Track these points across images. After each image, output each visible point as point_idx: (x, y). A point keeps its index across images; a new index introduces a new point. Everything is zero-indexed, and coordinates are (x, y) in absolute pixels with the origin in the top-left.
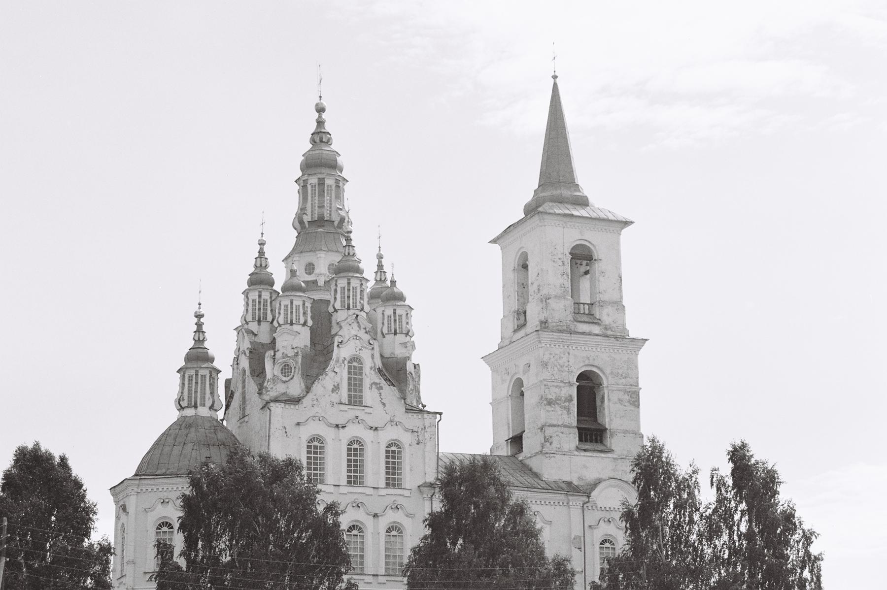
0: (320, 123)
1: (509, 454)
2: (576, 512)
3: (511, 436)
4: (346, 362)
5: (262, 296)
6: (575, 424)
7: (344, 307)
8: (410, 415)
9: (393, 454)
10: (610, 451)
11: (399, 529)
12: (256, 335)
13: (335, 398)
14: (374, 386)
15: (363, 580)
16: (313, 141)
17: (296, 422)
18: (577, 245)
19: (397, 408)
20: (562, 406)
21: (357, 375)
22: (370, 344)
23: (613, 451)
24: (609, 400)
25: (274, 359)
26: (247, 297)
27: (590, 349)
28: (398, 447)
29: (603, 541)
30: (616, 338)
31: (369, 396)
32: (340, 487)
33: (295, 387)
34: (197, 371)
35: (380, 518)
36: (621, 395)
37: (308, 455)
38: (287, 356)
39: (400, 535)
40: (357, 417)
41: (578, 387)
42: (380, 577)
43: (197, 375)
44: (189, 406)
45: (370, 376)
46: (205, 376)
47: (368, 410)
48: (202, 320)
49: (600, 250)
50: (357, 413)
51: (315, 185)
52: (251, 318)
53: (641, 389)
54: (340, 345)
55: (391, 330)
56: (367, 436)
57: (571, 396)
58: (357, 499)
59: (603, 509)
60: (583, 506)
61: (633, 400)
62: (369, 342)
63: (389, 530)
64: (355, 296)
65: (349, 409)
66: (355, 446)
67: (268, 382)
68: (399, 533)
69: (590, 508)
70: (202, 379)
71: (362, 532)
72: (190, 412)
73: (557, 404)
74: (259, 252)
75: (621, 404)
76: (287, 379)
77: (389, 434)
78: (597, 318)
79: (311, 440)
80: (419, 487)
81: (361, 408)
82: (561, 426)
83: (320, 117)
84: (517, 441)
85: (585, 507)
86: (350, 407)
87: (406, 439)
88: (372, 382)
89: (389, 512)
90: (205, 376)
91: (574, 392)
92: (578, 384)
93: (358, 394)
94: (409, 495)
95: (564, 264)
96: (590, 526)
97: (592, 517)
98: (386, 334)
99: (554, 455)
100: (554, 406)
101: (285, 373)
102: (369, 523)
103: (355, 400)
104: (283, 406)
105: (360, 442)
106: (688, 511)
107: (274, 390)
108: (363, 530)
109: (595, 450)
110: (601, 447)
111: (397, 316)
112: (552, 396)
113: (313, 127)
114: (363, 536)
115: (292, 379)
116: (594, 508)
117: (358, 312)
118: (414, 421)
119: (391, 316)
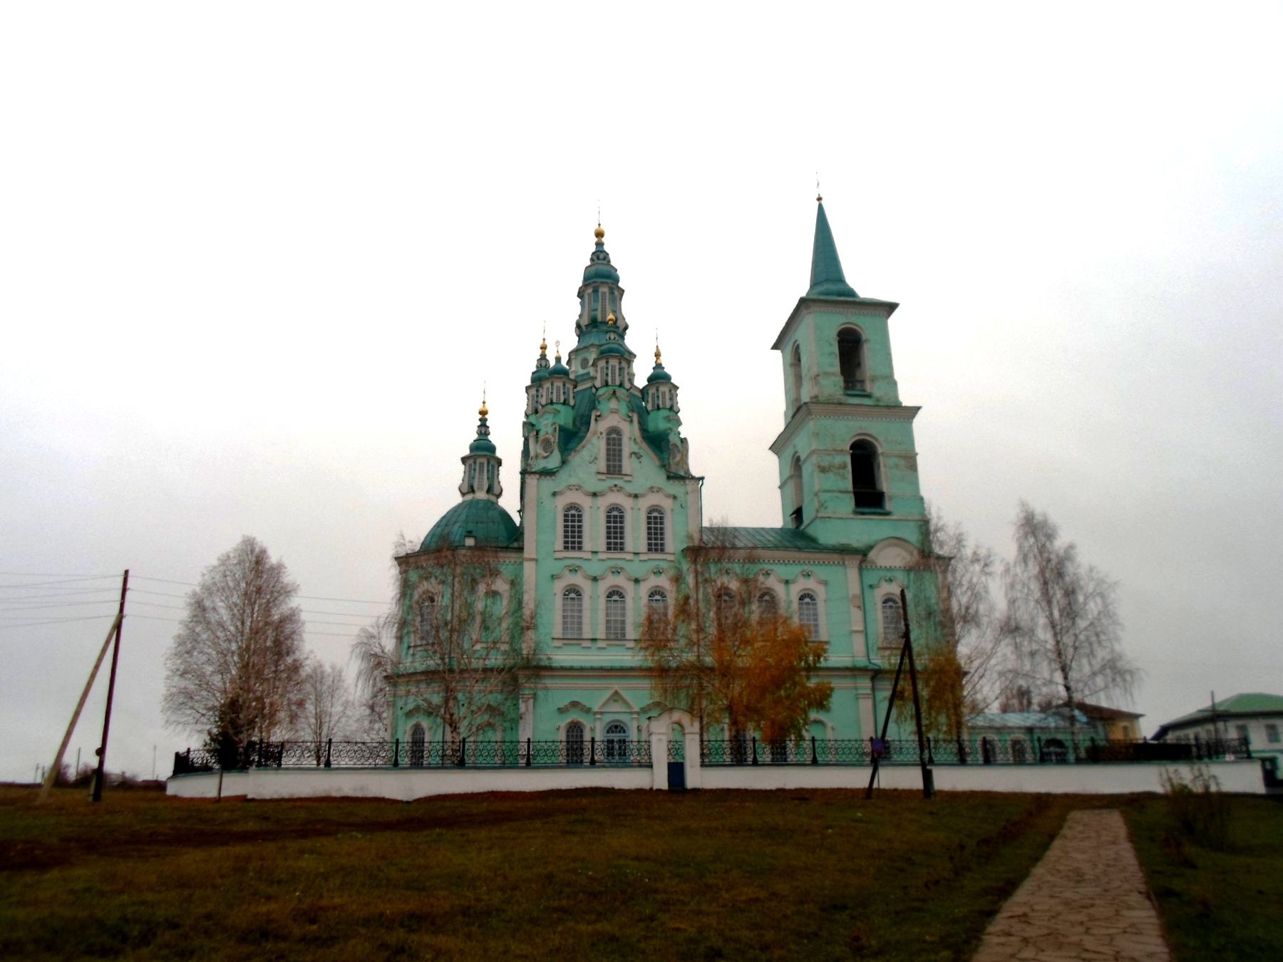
0: (599, 245)
2: (853, 573)
4: (604, 435)
8: (671, 482)
10: (888, 514)
11: (663, 593)
13: (594, 468)
14: (633, 456)
15: (624, 645)
16: (592, 260)
17: (552, 491)
19: (659, 479)
24: (885, 466)
25: (537, 438)
26: (528, 395)
28: (660, 512)
31: (628, 464)
33: (554, 461)
34: (475, 459)
36: (895, 460)
38: (547, 433)
40: (616, 486)
41: (852, 456)
44: (468, 493)
45: (627, 447)
48: (486, 416)
50: (617, 482)
63: (802, 598)
64: (613, 373)
66: (655, 514)
69: (869, 567)
70: (480, 467)
71: (623, 597)
72: (469, 497)
77: (653, 500)
79: (568, 508)
84: (798, 514)
85: (864, 566)
86: (609, 476)
87: (666, 504)
88: (632, 451)
89: (653, 577)
91: (848, 460)
97: (870, 578)
102: (629, 588)
103: (614, 467)
105: (620, 510)
107: (540, 465)
109: (792, 433)
111: (660, 393)
112: (825, 463)
113: (593, 249)
114: (624, 601)
115: (552, 453)
116: (874, 567)
118: (675, 488)
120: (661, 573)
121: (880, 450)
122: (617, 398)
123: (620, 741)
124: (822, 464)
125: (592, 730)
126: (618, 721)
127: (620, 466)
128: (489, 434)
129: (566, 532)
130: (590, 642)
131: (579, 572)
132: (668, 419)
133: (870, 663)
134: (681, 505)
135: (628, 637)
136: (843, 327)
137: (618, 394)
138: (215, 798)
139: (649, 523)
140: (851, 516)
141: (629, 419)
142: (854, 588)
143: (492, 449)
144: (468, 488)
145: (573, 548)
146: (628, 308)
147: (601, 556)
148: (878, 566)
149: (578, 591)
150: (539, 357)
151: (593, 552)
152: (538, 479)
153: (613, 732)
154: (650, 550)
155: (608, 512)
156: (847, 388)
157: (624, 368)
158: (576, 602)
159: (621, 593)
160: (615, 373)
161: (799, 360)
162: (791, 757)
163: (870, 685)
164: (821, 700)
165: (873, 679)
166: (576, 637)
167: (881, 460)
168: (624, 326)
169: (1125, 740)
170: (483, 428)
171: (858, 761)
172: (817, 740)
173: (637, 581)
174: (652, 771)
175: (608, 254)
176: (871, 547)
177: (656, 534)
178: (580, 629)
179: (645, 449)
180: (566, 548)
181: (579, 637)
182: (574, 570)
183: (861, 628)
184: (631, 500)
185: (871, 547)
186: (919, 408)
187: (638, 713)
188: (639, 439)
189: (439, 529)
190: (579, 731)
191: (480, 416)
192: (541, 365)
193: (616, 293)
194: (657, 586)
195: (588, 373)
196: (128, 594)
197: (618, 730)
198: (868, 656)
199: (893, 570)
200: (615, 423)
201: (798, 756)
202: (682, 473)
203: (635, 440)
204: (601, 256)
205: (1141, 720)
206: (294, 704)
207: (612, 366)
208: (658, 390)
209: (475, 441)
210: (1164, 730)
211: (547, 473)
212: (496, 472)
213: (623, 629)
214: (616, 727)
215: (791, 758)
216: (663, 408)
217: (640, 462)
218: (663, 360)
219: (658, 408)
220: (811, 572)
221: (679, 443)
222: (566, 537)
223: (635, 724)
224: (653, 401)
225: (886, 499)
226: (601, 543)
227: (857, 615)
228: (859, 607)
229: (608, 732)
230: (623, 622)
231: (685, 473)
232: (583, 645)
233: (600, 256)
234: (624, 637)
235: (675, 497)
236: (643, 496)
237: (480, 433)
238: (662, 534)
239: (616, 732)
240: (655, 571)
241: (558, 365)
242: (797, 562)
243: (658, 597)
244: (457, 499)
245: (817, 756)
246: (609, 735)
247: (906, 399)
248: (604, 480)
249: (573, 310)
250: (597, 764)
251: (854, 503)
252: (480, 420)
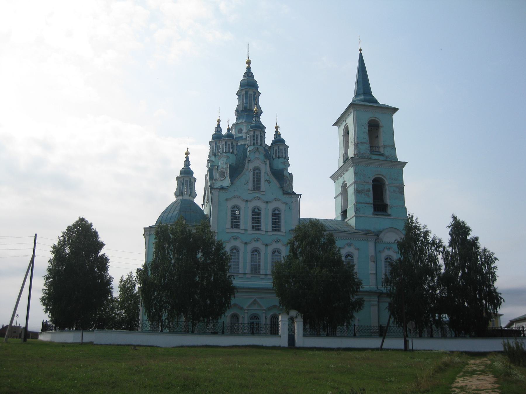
0: (249, 68)
1: (342, 219)
7: (252, 144)
8: (285, 196)
9: (276, 215)
10: (389, 215)
11: (279, 252)
12: (213, 162)
14: (266, 182)
18: (370, 120)
22: (265, 162)
25: (217, 170)
28: (279, 211)
29: (386, 258)
30: (391, 161)
31: (263, 186)
32: (248, 231)
37: (273, 226)
38: (223, 168)
40: (257, 197)
41: (373, 185)
42: (268, 276)
43: (183, 180)
44: (179, 195)
47: (263, 193)
49: (382, 122)
54: (249, 162)
55: (277, 156)
56: (262, 206)
57: (369, 189)
62: (264, 161)
65: (253, 192)
66: (256, 211)
67: (214, 181)
69: (379, 242)
70: (186, 183)
74: (217, 125)
75: (395, 193)
76: (223, 179)
77: (275, 205)
79: (233, 207)
80: (290, 231)
81: (259, 192)
82: (365, 203)
85: (377, 242)
86: (254, 192)
87: (282, 207)
88: (266, 179)
94: (284, 235)
95: (365, 128)
96: (380, 251)
98: (275, 158)
100: (361, 194)
101: (222, 176)
103: (256, 188)
106: (160, 296)
107: (218, 185)
110: (385, 214)
113: (245, 70)
115: (225, 178)
116: (382, 242)
117: (259, 147)
118: (286, 199)
119: (277, 150)
120: (279, 242)
121: (387, 183)
122: (259, 151)
123: (256, 324)
124: (359, 189)
125: (243, 318)
126: (255, 314)
127: (260, 187)
131: (259, 241)
132: (283, 163)
133: (378, 289)
134: (289, 208)
135: (261, 273)
137: (259, 150)
138: (79, 343)
139: (273, 216)
140: (372, 216)
141: (265, 163)
143: (192, 173)
144: (179, 193)
145: (235, 228)
146: (262, 102)
148: (384, 241)
149: (238, 249)
151: (266, 231)
152: (219, 192)
153: (253, 319)
154: (273, 230)
155: (253, 210)
157: (262, 136)
158: (236, 255)
160: (258, 139)
161: (348, 133)
162: (338, 333)
163: (377, 300)
164: (359, 305)
165: (379, 297)
166: (236, 272)
167: (387, 187)
168: (260, 112)
169: (493, 328)
170: (187, 163)
171: (362, 335)
173: (267, 245)
176: (381, 232)
177: (276, 222)
179: (273, 179)
180: (232, 227)
181: (238, 272)
182: (257, 240)
183: (374, 272)
185: (381, 232)
186: (407, 162)
188: (270, 173)
189: (166, 214)
190: (237, 318)
191: (186, 156)
193: (257, 95)
196: (36, 245)
197: (256, 318)
199: (391, 244)
200: (257, 165)
202: (289, 191)
203: (267, 173)
204: (250, 75)
205: (501, 317)
207: (257, 135)
209: (183, 168)
210: (512, 323)
212: (193, 185)
213: (259, 269)
214: (255, 317)
216: (281, 158)
217: (270, 185)
218: (281, 131)
219: (279, 158)
222: (232, 222)
223: (264, 315)
224: (276, 153)
225: (389, 208)
226: (270, 227)
227: (372, 265)
228: (374, 262)
229: (251, 319)
230: (259, 266)
231: (291, 191)
232: (239, 276)
233: (249, 74)
235: (286, 204)
236: (271, 202)
238: (279, 222)
239: (255, 319)
243: (276, 254)
244: (173, 199)
245: (356, 333)
246: (251, 320)
247: (400, 158)
248: (252, 194)
249: (234, 103)
251: (373, 209)
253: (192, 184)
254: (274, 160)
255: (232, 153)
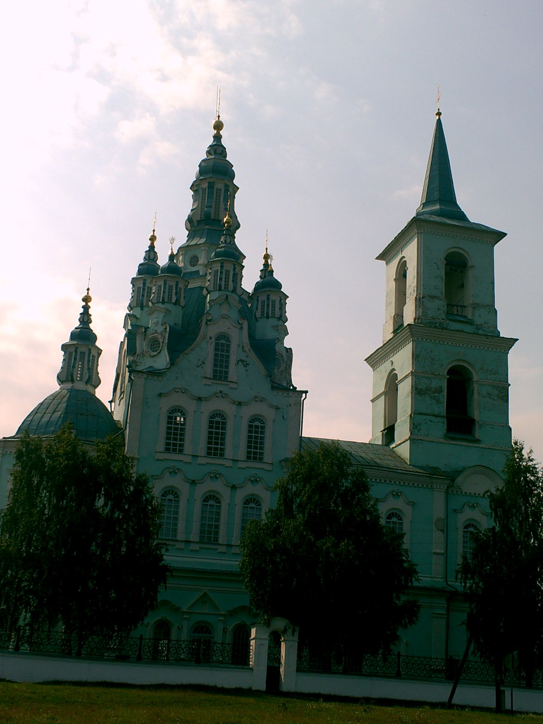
0: (218, 138)
3: (387, 426)
4: (213, 339)
5: (147, 284)
6: (443, 411)
8: (275, 392)
10: (478, 441)
11: (258, 501)
15: (217, 549)
20: (432, 396)
21: (224, 352)
22: (240, 323)
23: (480, 440)
27: (461, 345)
28: (262, 422)
31: (233, 371)
32: (199, 458)
35: (238, 489)
38: (156, 332)
39: (176, 499)
40: (221, 392)
41: (449, 380)
43: (76, 351)
45: (234, 355)
46: (84, 353)
51: (206, 189)
52: (135, 304)
53: (510, 385)
54: (208, 323)
55: (264, 315)
58: (215, 470)
59: (468, 494)
60: (447, 490)
61: (502, 395)
63: (206, 499)
65: (213, 383)
67: (138, 357)
68: (257, 506)
69: (455, 492)
73: (427, 394)
74: (149, 247)
76: (155, 353)
78: (469, 318)
79: (172, 411)
80: (281, 461)
82: (430, 415)
83: (218, 133)
85: (450, 491)
86: (215, 381)
87: (269, 414)
88: (238, 359)
90: (84, 353)
91: (444, 385)
92: (448, 377)
93: (224, 370)
94: (270, 469)
95: (438, 269)
98: (259, 318)
99: (422, 441)
100: (423, 396)
104: (146, 377)
107: (145, 364)
108: (220, 501)
113: (210, 141)
114: (402, 524)
115: (159, 353)
116: (459, 493)
117: (228, 293)
119: (264, 302)
121: (475, 378)
125: (180, 629)
127: (227, 373)
128: (91, 322)
129: (168, 433)
130: (183, 544)
132: (276, 328)
135: (220, 541)
136: (449, 251)
142: (439, 512)
147: (201, 461)
149: (176, 493)
150: (148, 249)
154: (249, 458)
155: (211, 418)
156: (448, 313)
159: (217, 499)
162: (366, 667)
172: (401, 656)
173: (234, 487)
174: (252, 672)
175: (225, 149)
176: (458, 472)
178: (175, 531)
180: (167, 450)
184: (234, 407)
185: (458, 472)
187: (224, 616)
188: (248, 347)
191: (84, 304)
192: (149, 257)
194: (253, 495)
195: (198, 272)
198: (446, 578)
201: (384, 669)
204: (219, 150)
206: (250, 606)
208: (268, 298)
211: (153, 373)
215: (365, 669)
216: (272, 317)
218: (274, 265)
220: (401, 492)
221: (284, 353)
224: (263, 308)
225: (477, 426)
227: (438, 536)
229: (194, 632)
234: (217, 541)
235: (277, 408)
236: (247, 404)
237: (82, 320)
240: (252, 479)
241: (172, 264)
242: (388, 482)
243: (252, 505)
244: (55, 387)
247: (504, 331)
250: (131, 659)
251: (445, 427)
252: (83, 307)
253: (93, 360)
254: (257, 320)
255: (175, 304)
